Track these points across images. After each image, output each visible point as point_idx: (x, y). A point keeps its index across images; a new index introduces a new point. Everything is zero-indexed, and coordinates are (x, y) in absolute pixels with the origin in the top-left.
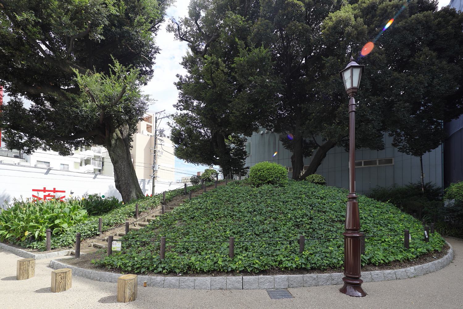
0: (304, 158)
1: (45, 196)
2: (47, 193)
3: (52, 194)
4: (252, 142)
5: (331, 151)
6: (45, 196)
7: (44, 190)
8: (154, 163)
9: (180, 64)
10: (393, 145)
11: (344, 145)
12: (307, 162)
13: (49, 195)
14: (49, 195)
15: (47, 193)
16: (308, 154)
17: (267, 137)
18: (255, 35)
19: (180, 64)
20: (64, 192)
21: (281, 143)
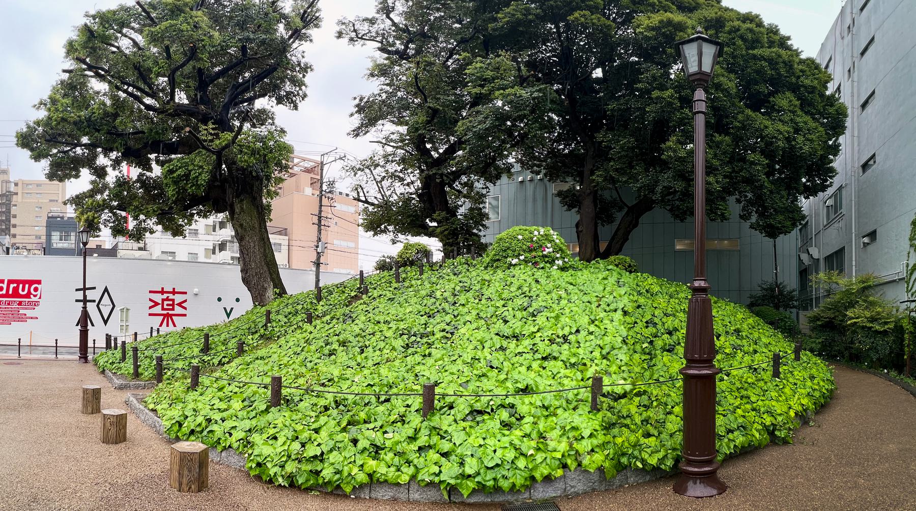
0: (600, 227)
1: (163, 300)
2: (165, 296)
3: (171, 296)
4: (499, 197)
5: (645, 219)
6: (163, 300)
7: (162, 292)
8: (319, 240)
9: (311, 41)
10: (741, 217)
11: (668, 208)
12: (606, 232)
13: (167, 299)
14: (167, 299)
15: (165, 296)
16: (610, 220)
17: (530, 187)
18: (262, 139)
19: (311, 41)
20: (150, 315)
21: (558, 199)
